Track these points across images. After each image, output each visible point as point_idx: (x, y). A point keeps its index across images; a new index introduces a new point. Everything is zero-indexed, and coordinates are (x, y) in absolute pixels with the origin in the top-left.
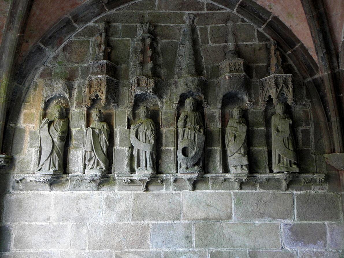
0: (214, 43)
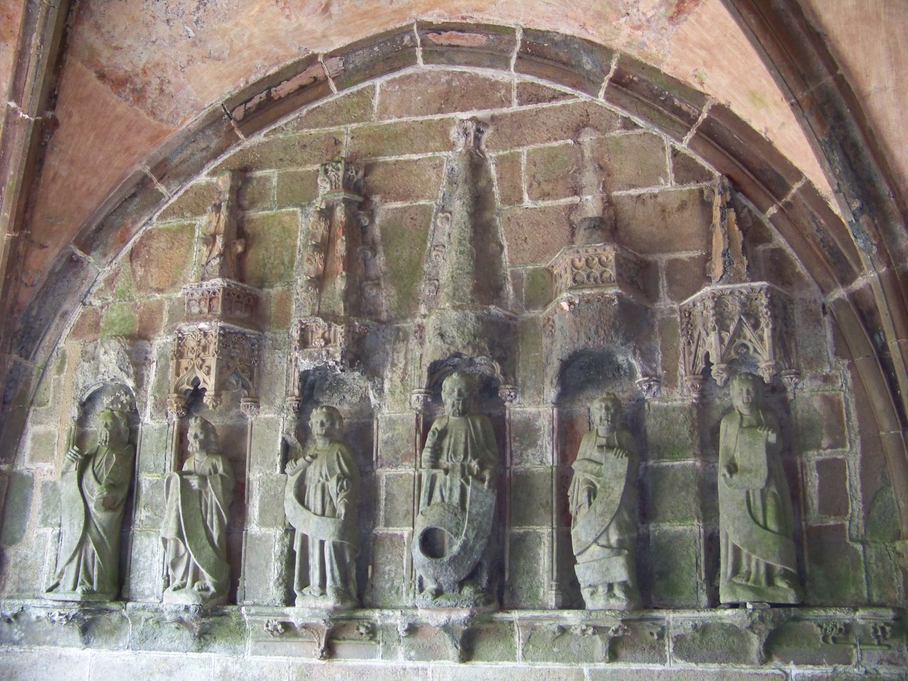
0: (539, 198)
